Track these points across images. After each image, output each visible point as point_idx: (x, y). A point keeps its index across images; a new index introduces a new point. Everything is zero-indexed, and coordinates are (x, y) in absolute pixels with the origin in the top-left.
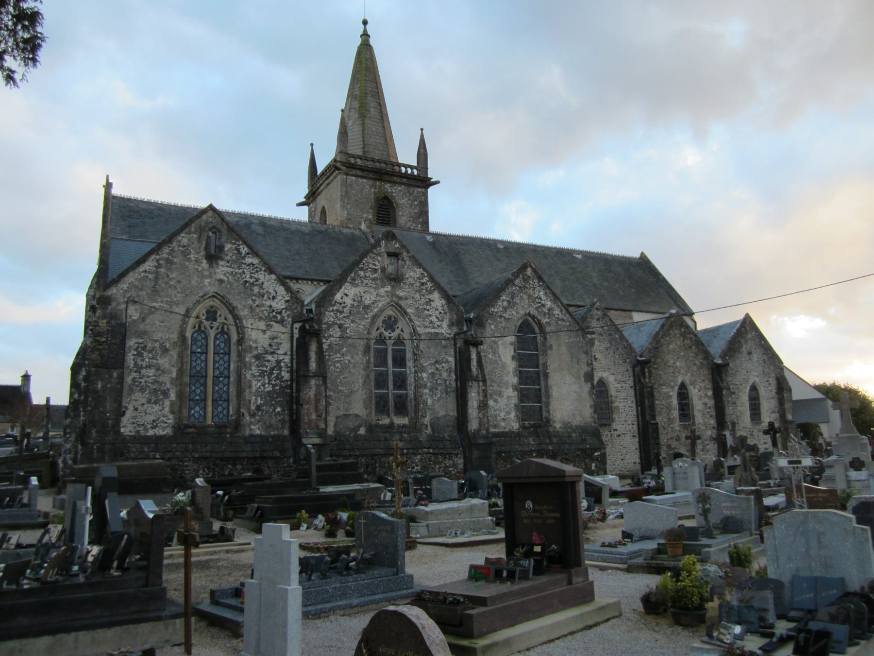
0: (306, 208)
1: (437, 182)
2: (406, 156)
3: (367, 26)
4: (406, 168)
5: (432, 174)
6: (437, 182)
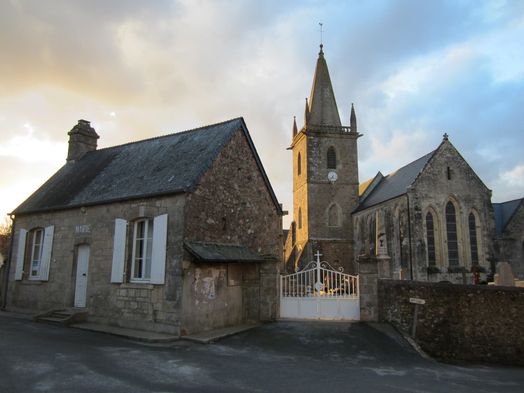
0: (291, 151)
1: (362, 135)
2: (345, 121)
6: (362, 135)
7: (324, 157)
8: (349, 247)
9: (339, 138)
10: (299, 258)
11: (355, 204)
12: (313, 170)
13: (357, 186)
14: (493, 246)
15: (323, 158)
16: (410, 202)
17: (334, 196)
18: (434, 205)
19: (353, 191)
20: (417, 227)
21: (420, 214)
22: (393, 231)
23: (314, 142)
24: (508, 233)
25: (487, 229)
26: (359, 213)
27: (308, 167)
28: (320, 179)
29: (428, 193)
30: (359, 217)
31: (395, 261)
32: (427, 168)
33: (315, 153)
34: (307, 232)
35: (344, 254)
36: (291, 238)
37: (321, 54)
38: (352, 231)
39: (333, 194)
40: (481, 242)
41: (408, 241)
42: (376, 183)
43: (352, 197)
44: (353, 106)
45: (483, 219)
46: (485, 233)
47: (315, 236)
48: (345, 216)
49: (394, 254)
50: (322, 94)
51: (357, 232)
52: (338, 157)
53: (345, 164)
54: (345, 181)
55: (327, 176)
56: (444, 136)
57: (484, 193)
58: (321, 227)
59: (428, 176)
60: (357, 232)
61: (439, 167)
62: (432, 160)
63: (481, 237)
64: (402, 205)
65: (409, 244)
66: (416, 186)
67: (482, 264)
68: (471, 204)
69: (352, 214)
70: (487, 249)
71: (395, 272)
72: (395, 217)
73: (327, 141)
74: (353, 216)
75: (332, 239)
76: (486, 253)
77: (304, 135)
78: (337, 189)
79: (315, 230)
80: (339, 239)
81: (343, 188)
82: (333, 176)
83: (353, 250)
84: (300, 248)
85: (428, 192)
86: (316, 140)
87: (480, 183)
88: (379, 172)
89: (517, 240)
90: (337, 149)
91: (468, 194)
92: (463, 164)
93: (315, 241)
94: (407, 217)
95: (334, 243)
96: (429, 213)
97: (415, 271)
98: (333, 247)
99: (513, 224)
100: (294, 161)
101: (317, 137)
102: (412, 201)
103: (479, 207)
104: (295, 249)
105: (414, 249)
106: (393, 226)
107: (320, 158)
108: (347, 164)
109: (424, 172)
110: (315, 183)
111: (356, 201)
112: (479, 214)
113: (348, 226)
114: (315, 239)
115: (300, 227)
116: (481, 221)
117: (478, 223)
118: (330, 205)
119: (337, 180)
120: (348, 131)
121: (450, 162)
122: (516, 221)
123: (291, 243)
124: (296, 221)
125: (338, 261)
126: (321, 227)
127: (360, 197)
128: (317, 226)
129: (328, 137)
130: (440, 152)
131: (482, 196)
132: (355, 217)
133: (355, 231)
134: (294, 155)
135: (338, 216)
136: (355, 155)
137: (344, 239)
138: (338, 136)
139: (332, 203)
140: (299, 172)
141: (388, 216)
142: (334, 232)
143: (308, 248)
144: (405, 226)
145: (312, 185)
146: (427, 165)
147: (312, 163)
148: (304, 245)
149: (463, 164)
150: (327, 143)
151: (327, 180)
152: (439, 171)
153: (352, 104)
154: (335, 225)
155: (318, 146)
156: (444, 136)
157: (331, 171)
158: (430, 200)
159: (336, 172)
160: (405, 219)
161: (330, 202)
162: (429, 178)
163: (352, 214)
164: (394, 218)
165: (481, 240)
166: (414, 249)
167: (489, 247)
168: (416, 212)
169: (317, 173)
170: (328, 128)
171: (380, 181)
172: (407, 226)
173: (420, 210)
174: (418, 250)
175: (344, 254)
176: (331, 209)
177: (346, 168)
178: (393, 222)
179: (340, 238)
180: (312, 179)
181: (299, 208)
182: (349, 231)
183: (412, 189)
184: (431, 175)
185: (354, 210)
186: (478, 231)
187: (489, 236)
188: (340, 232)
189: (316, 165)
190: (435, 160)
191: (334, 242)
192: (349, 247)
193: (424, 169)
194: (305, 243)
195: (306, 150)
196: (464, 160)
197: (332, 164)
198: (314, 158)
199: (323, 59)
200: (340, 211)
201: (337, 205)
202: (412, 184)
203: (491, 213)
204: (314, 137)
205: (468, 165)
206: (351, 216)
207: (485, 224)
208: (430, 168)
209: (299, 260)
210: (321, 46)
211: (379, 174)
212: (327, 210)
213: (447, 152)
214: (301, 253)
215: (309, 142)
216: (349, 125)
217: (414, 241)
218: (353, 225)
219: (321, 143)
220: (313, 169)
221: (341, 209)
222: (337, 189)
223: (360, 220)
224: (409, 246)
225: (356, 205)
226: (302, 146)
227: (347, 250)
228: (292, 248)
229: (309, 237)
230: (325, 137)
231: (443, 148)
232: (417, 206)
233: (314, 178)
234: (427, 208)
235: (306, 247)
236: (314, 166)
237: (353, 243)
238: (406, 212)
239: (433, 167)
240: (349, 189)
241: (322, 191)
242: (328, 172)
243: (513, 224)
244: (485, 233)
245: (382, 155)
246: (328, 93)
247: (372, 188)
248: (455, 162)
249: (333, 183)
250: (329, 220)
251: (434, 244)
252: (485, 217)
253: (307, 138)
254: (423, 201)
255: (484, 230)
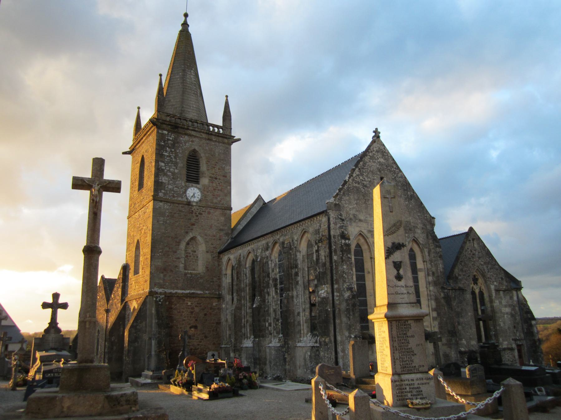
0: (130, 156)
1: (239, 140)
2: (215, 117)
3: (188, 19)
4: (218, 129)
5: (235, 132)
6: (239, 140)
7: (182, 164)
8: (214, 304)
9: (206, 139)
10: (131, 321)
11: (225, 238)
12: (164, 181)
13: (228, 211)
14: (444, 298)
15: (180, 165)
16: (332, 226)
17: (193, 225)
18: (365, 232)
19: (222, 219)
20: (345, 267)
21: (348, 245)
22: (297, 274)
23: (168, 140)
24: (456, 279)
25: (433, 273)
26: (233, 251)
27: (157, 175)
28: (174, 197)
29: (357, 213)
30: (232, 257)
31: (299, 324)
32: (354, 175)
33: (167, 156)
34: (148, 278)
35: (205, 315)
36: (120, 290)
37: (185, 25)
38: (220, 279)
39: (193, 220)
40: (426, 293)
41: (330, 290)
42: (254, 211)
43: (222, 227)
44: (227, 100)
45: (427, 258)
46: (430, 278)
47: (161, 286)
48: (209, 256)
49: (299, 314)
50: (183, 78)
51: (227, 281)
52: (203, 167)
53: (213, 179)
54: (212, 203)
55: (185, 192)
56: (374, 132)
57: (426, 220)
58: (172, 271)
59: (356, 187)
60: (227, 281)
61: (370, 175)
62: (361, 163)
63: (425, 285)
64: (317, 232)
65: (331, 296)
66: (340, 199)
67: (428, 327)
68: (411, 235)
69: (221, 253)
70: (433, 304)
71: (299, 344)
72: (300, 252)
73: (189, 141)
74: (221, 255)
75: (188, 291)
76: (434, 310)
77: (154, 127)
78: (200, 214)
79: (162, 275)
80: (199, 292)
81: (209, 213)
82: (194, 193)
83: (220, 309)
84: (134, 305)
85: (357, 211)
86: (172, 137)
87: (420, 206)
88: (260, 195)
89: (466, 290)
90: (202, 155)
91: (408, 220)
92: (399, 175)
93: (161, 293)
94: (328, 250)
95: (190, 297)
96: (358, 245)
97: (343, 342)
98: (189, 304)
99: (460, 267)
100: (133, 170)
101: (174, 132)
102: (335, 224)
103: (421, 240)
104: (125, 307)
105: (340, 304)
106: (296, 266)
107: (176, 164)
108: (216, 178)
109: (350, 180)
110: (166, 201)
111: (227, 234)
112: (422, 251)
113: (214, 271)
114: (160, 290)
115: (136, 272)
116: (424, 262)
117: (420, 265)
118: (188, 238)
119: (200, 201)
120: (219, 131)
121: (383, 170)
122: (463, 263)
123: (119, 298)
124: (129, 262)
125: (196, 327)
126: (172, 271)
127: (233, 230)
128: (165, 269)
129: (190, 135)
130: (370, 154)
131: (424, 225)
132: (225, 258)
133: (224, 279)
134: (133, 162)
135: (199, 256)
136: (228, 167)
137: (207, 292)
138: (204, 136)
139: (191, 235)
140: (141, 185)
141: (288, 250)
142: (192, 281)
143: (148, 306)
144: (324, 264)
145: (161, 204)
146: (354, 170)
147: (163, 170)
148: (142, 300)
149: (399, 175)
150: (188, 143)
151: (184, 199)
152: (370, 181)
153: (227, 96)
154: (194, 270)
155: (173, 146)
156: (374, 132)
157: (192, 186)
158: (360, 224)
159: (199, 189)
160: (323, 253)
161: (187, 233)
162: (358, 189)
163: (221, 253)
164: (298, 254)
165: (425, 289)
166: (340, 304)
167: (437, 300)
168: (343, 241)
169: (170, 187)
170: (190, 123)
171: (262, 208)
172: (328, 264)
173: (349, 239)
174: (348, 305)
175: (205, 315)
176: (188, 244)
177: (214, 185)
178: (296, 260)
179: (201, 290)
180: (161, 194)
181: (136, 241)
182: (215, 279)
183: (336, 205)
184: (360, 186)
185: (223, 247)
186: (421, 275)
187: (435, 284)
188: (201, 281)
189: (169, 174)
190: (365, 164)
191: (191, 296)
192: (214, 304)
193: (351, 176)
194: (144, 297)
195: (154, 150)
196: (400, 171)
197: (193, 177)
198: (167, 164)
199: (188, 32)
200: (202, 248)
201: (199, 238)
202: (335, 197)
203: (438, 250)
204: (169, 131)
205: (405, 177)
206: (219, 257)
207: (429, 266)
208: (358, 175)
209: (132, 327)
210: (186, 15)
211: (259, 198)
212: (183, 245)
213: (380, 155)
214: (135, 314)
215: (160, 138)
216: (220, 123)
217: (339, 290)
218: (220, 271)
219: (178, 143)
220: (164, 179)
221: (204, 245)
222: (200, 214)
223: (233, 262)
224: (331, 298)
225: (226, 240)
226: (149, 147)
227: (211, 308)
228: (120, 306)
229: (150, 288)
230: (186, 134)
231: (375, 149)
232: (343, 232)
233: (165, 194)
234: (355, 237)
235: (144, 303)
236: (165, 175)
237: (220, 297)
238: (326, 242)
239: (362, 175)
240: (216, 216)
241: (176, 215)
242: (187, 187)
243: (460, 267)
244: (430, 278)
245: (272, 165)
246: (192, 76)
247: (250, 217)
248: (390, 171)
249: (194, 204)
250: (185, 261)
251: (365, 296)
252: (429, 255)
253: (158, 132)
254: (351, 225)
255: (428, 275)
